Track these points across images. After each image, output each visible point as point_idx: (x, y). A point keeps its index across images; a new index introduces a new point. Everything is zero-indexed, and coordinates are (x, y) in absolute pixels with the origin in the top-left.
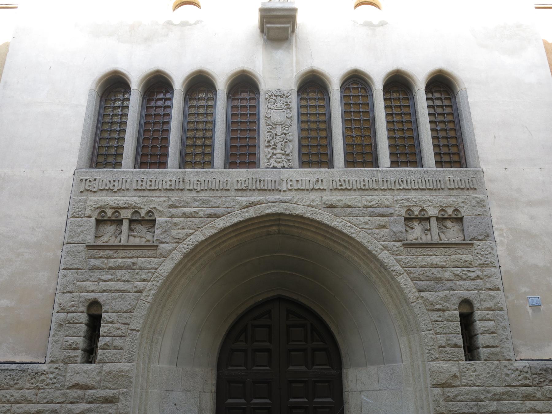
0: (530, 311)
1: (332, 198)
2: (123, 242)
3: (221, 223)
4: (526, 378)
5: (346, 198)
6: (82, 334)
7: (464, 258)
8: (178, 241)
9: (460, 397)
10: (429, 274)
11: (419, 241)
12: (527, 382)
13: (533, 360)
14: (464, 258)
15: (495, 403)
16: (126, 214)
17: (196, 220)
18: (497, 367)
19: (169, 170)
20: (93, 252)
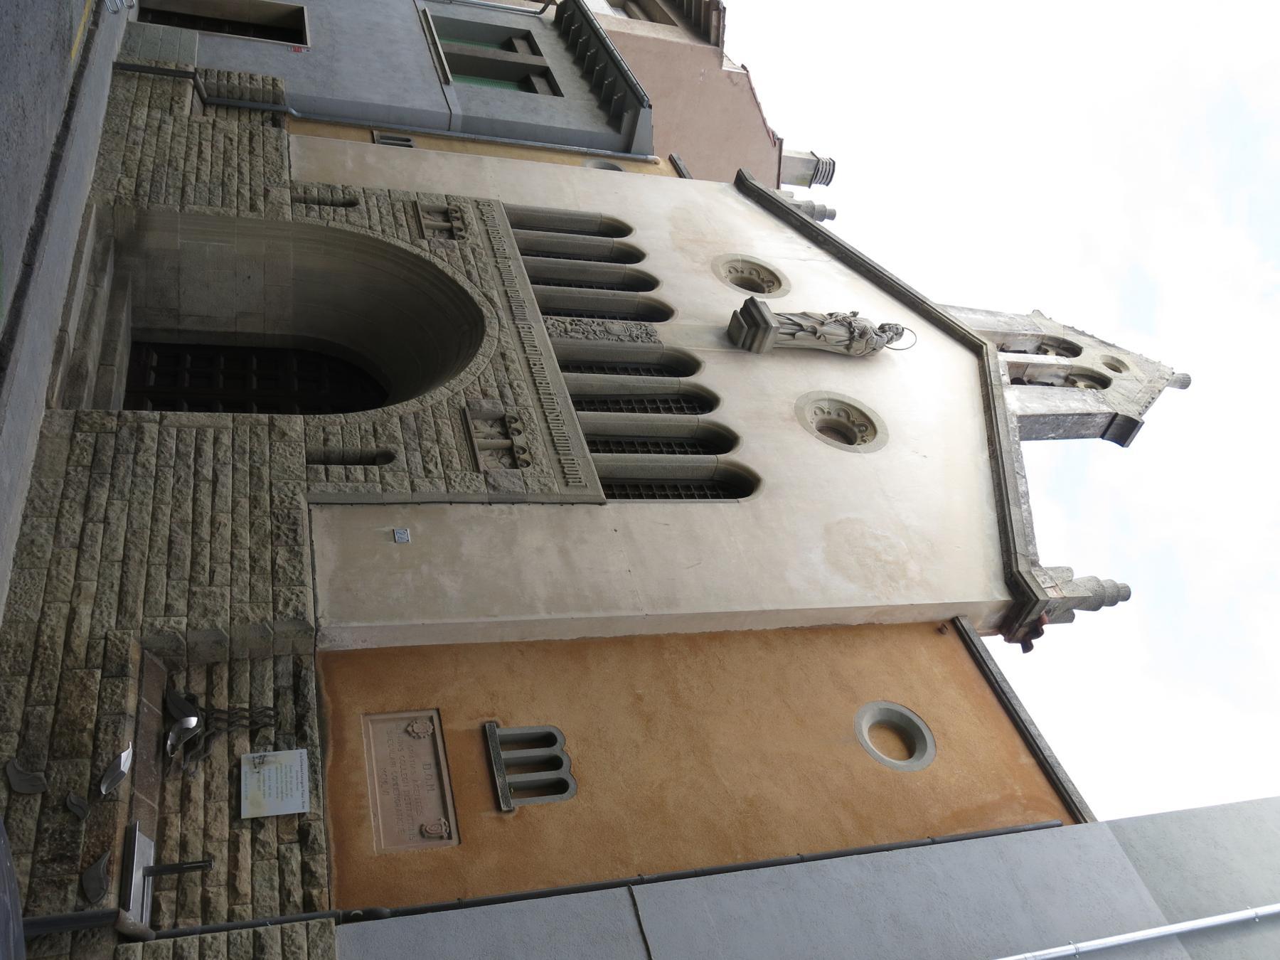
0: (387, 529)
1: (515, 354)
2: (424, 222)
3: (461, 279)
4: (282, 502)
5: (518, 367)
6: (349, 447)
7: (456, 461)
8: (435, 254)
9: (255, 439)
10: (425, 426)
11: (474, 434)
12: (277, 502)
13: (310, 522)
14: (456, 461)
15: (247, 469)
16: (519, 440)
17: (461, 263)
18: (300, 477)
19: (561, 374)
20: (409, 209)
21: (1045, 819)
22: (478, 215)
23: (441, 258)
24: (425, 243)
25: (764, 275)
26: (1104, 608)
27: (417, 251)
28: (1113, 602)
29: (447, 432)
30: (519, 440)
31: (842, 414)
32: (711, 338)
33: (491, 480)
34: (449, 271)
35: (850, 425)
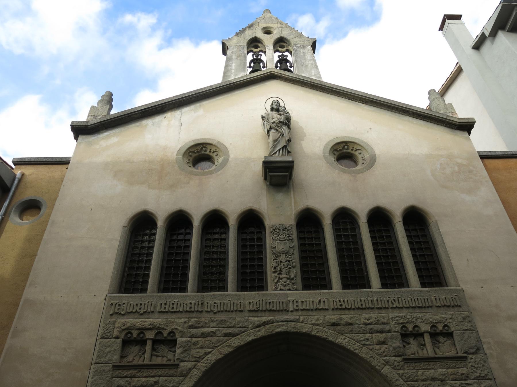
1: (334, 317)
2: (146, 362)
3: (236, 342)
7: (460, 371)
17: (214, 339)
20: (118, 372)
21: (28, 170)
22: (136, 315)
23: (207, 354)
24: (185, 366)
25: (198, 149)
26: (113, 103)
27: (196, 374)
28: (112, 100)
29: (431, 373)
30: (425, 328)
31: (191, 154)
32: (280, 196)
33: (472, 351)
34: (226, 350)
35: (340, 152)
